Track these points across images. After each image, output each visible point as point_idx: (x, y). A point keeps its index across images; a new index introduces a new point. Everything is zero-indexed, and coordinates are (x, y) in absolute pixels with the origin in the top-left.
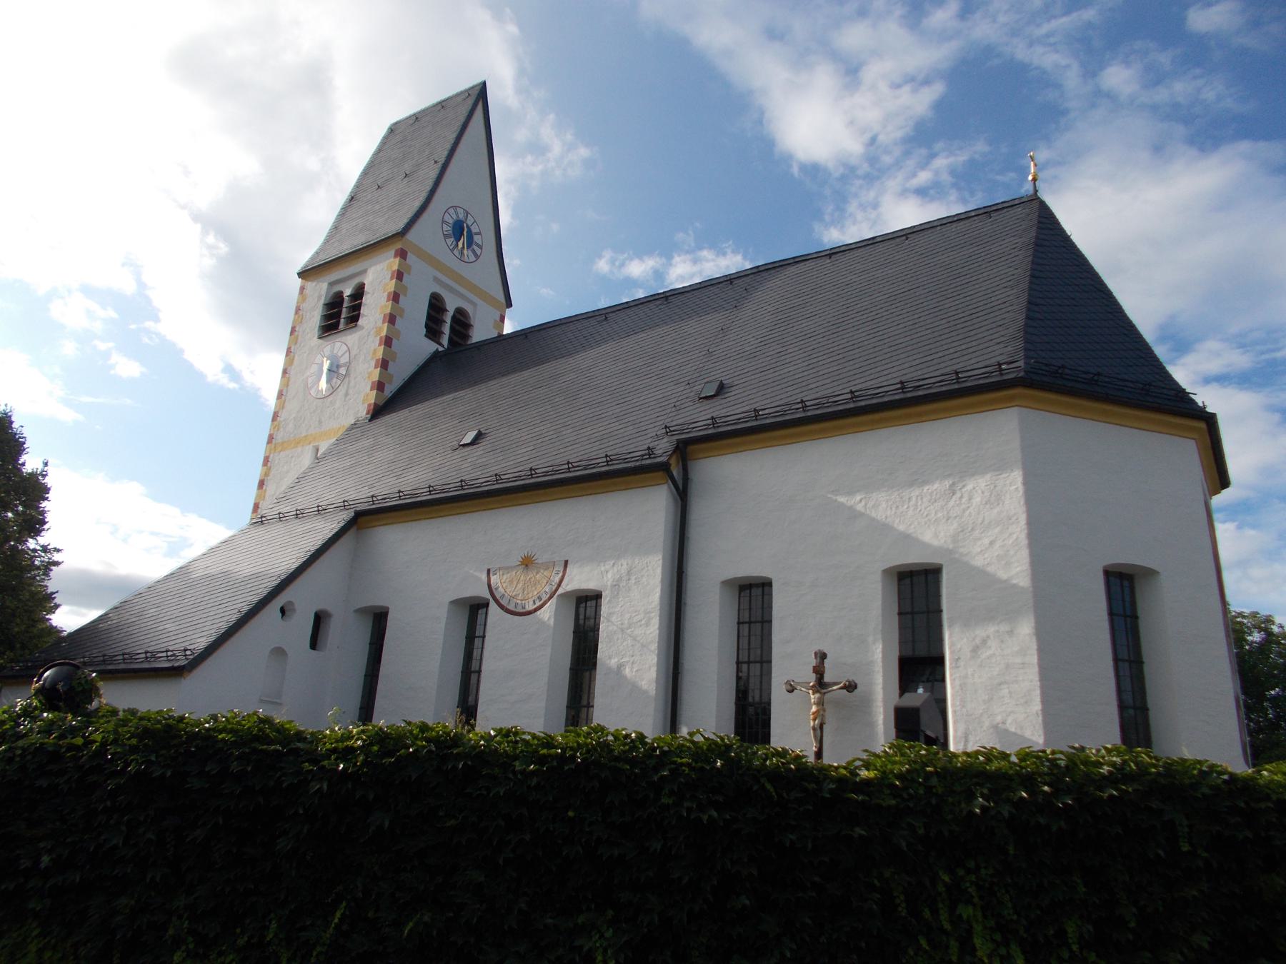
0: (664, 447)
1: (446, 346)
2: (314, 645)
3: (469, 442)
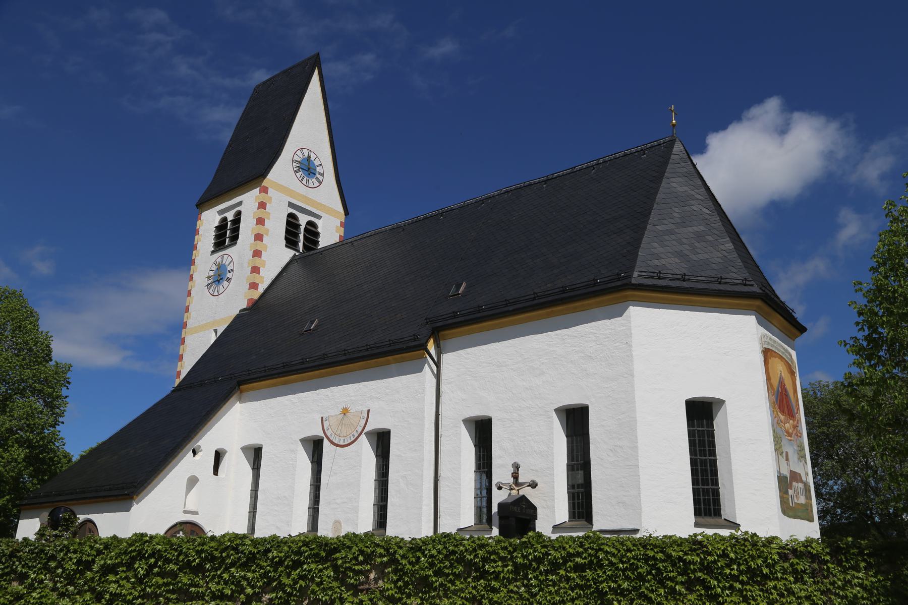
1: (301, 251)
2: (216, 471)
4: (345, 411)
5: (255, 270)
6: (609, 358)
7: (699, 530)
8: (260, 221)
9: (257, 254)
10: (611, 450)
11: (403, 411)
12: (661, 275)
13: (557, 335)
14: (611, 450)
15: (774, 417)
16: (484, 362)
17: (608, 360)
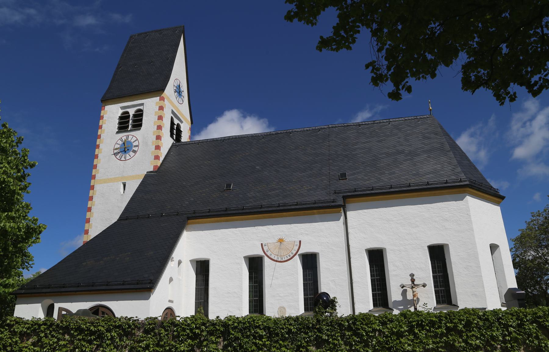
4: (281, 241)
5: (158, 148)
6: (458, 221)
10: (465, 268)
11: (328, 243)
12: (476, 182)
13: (424, 207)
14: (465, 268)
16: (377, 218)
17: (457, 222)
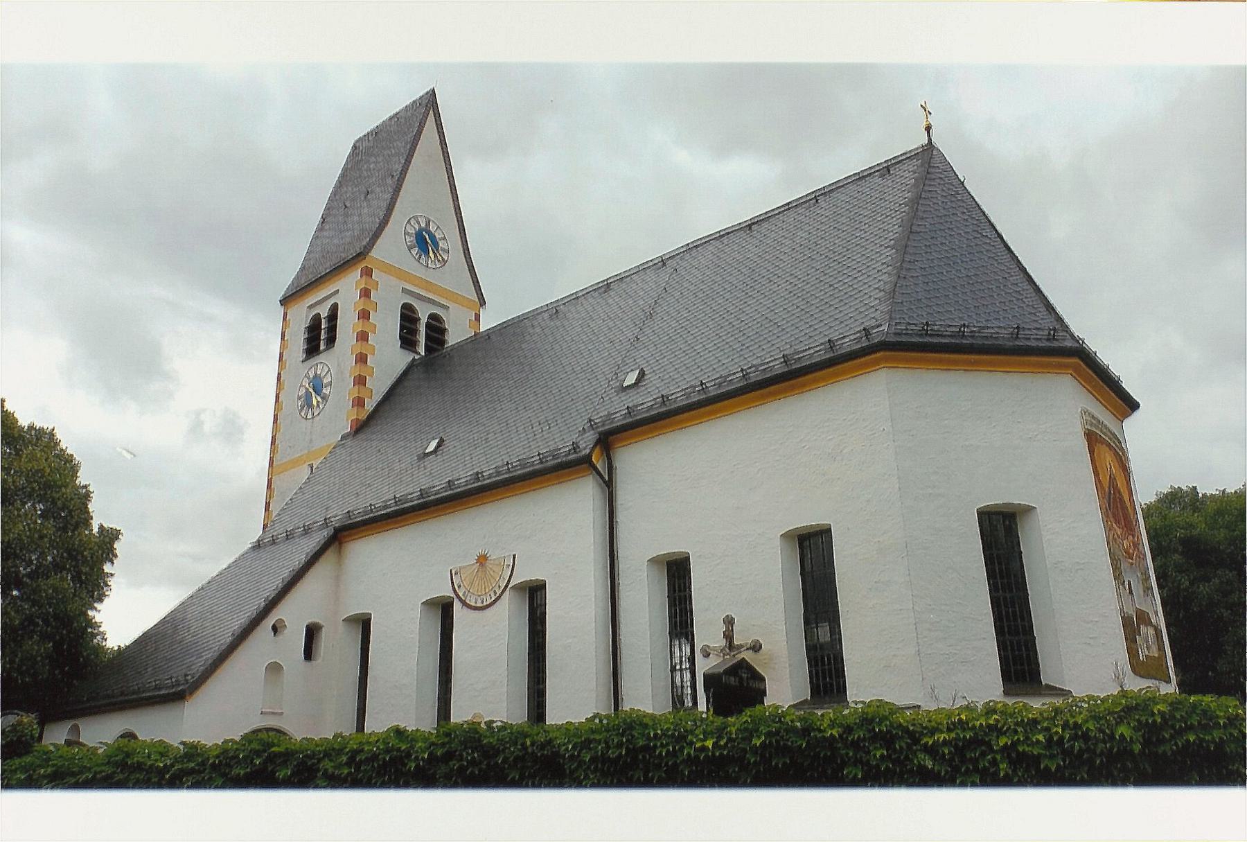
0: (587, 442)
2: (309, 654)
3: (633, 382)
4: (482, 559)
7: (1010, 701)
8: (364, 315)
9: (362, 359)
15: (1109, 529)
